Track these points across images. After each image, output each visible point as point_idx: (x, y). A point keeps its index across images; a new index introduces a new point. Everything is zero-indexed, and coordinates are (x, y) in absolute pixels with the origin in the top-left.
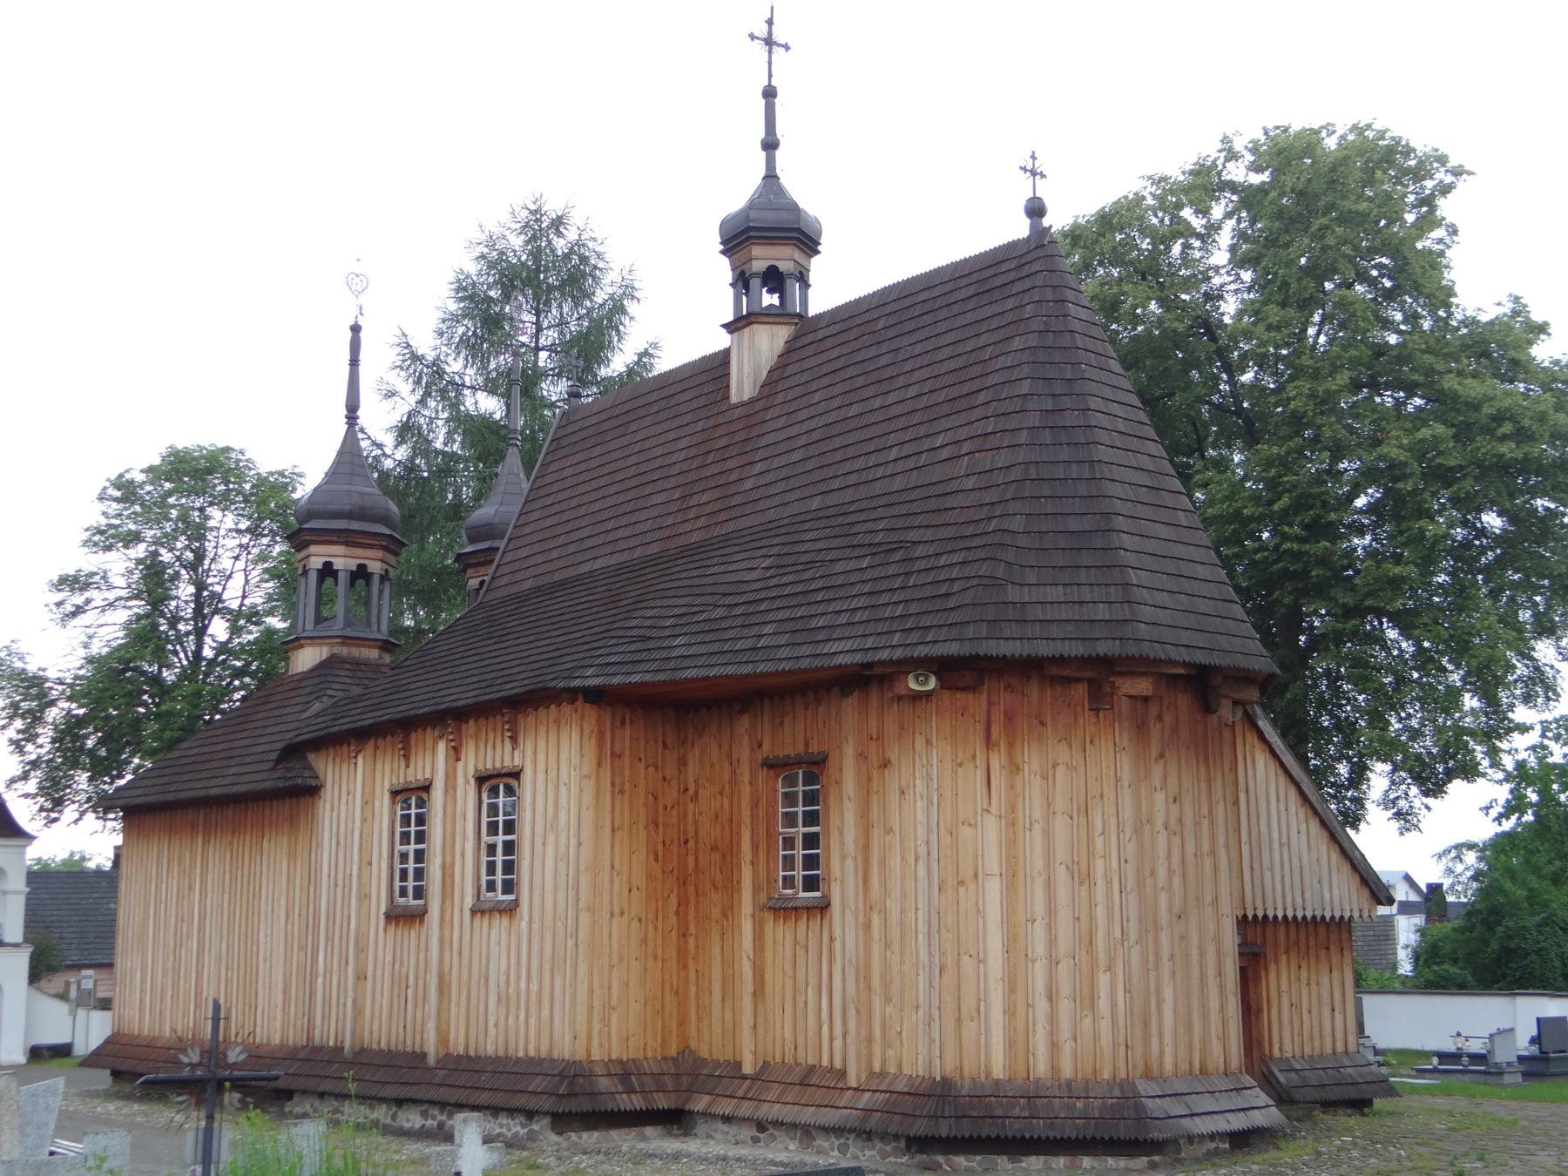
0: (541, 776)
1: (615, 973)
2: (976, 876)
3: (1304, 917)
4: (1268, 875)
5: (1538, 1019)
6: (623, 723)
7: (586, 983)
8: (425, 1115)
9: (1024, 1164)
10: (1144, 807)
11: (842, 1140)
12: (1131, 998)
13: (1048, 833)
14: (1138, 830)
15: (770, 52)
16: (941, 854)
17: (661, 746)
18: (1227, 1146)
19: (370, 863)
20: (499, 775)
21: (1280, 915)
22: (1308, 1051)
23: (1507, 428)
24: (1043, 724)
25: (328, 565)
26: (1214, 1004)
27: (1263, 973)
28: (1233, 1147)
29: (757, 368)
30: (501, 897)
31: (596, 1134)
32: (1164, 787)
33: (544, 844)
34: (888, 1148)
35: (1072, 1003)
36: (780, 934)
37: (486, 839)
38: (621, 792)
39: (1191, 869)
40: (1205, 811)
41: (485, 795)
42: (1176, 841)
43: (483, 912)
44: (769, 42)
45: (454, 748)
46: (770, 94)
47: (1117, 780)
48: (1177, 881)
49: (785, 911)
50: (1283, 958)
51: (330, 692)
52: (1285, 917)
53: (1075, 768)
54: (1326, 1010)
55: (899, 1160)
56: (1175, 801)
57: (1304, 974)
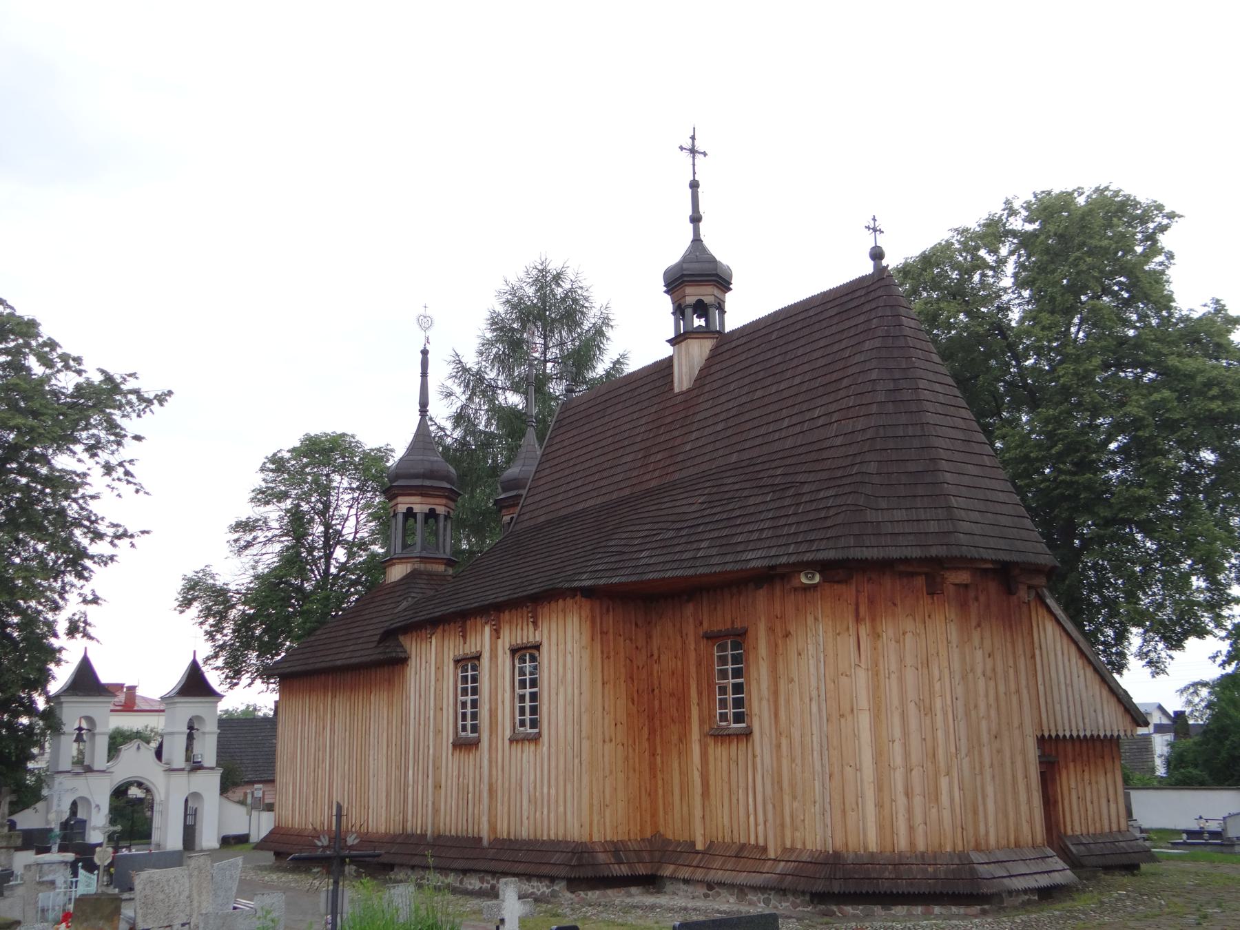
0: (554, 648)
1: (607, 781)
2: (852, 711)
6: (608, 610)
8: (482, 880)
11: (766, 896)
12: (964, 794)
13: (901, 680)
15: (694, 158)
16: (828, 696)
18: (1036, 898)
19: (442, 709)
20: (526, 648)
21: (1054, 735)
23: (1215, 391)
24: (895, 604)
25: (410, 510)
26: (1023, 797)
27: (1058, 778)
29: (691, 368)
30: (530, 731)
31: (597, 892)
33: (557, 694)
34: (798, 901)
35: (922, 797)
36: (718, 753)
37: (518, 691)
38: (608, 657)
41: (517, 662)
43: (517, 741)
44: (693, 151)
45: (495, 630)
46: (694, 185)
47: (949, 642)
48: (993, 713)
49: (722, 737)
50: (1071, 765)
51: (413, 595)
53: (919, 635)
54: (1104, 801)
56: (989, 656)
57: (1087, 777)
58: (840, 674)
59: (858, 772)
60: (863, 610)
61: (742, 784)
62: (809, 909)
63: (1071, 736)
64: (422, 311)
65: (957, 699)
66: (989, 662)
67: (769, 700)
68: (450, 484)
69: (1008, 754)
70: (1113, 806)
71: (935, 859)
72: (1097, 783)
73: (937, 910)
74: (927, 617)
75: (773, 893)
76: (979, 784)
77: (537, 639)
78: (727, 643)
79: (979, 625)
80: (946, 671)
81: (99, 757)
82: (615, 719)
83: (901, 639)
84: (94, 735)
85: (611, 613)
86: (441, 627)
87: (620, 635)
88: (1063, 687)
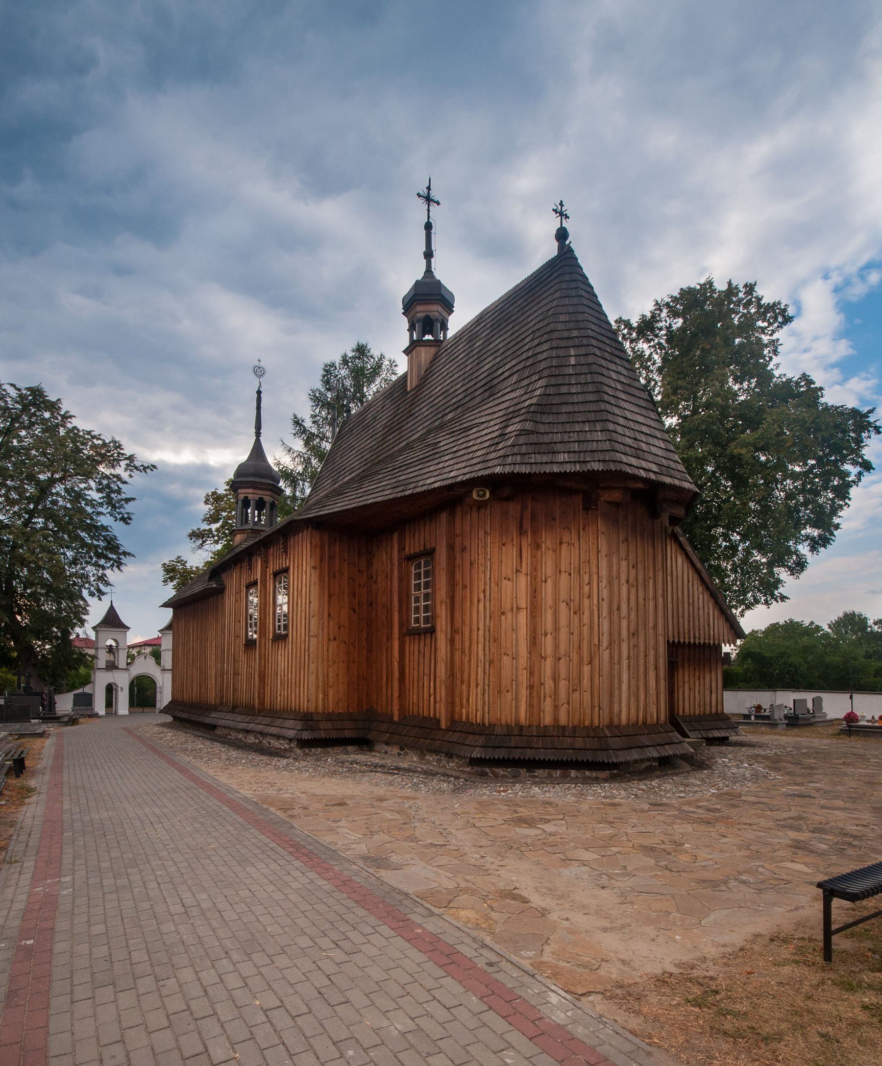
1: (331, 669)
3: (699, 643)
4: (681, 620)
5: (794, 700)
6: (335, 541)
7: (314, 674)
8: (256, 738)
9: (536, 774)
10: (615, 569)
11: (439, 757)
12: (603, 679)
13: (556, 584)
14: (610, 582)
16: (492, 597)
17: (357, 554)
18: (657, 764)
19: (240, 621)
22: (697, 712)
24: (554, 519)
25: (246, 498)
26: (652, 683)
27: (676, 673)
28: (660, 765)
29: (419, 371)
31: (319, 749)
32: (627, 559)
34: (461, 762)
35: (567, 682)
38: (334, 576)
39: (641, 607)
40: (651, 575)
42: (633, 590)
44: (428, 199)
46: (428, 227)
47: (598, 552)
48: (633, 614)
50: (686, 665)
52: (689, 642)
53: (573, 544)
54: (707, 692)
55: (466, 769)
56: (633, 567)
57: (697, 674)
58: (503, 578)
59: (514, 661)
60: (527, 524)
61: (427, 671)
62: (469, 769)
63: (689, 642)
64: (257, 363)
65: (603, 600)
66: (633, 572)
67: (446, 603)
68: (272, 480)
69: (642, 649)
70: (714, 696)
71: (575, 732)
72: (704, 678)
73: (573, 773)
74: (581, 530)
75: (443, 755)
76: (616, 672)
77: (288, 565)
78: (421, 562)
79: (626, 540)
80: (595, 576)
81: (122, 661)
82: (338, 623)
83: (558, 549)
84: (118, 649)
85: (338, 543)
86: (239, 565)
87: (345, 560)
88: (686, 605)
